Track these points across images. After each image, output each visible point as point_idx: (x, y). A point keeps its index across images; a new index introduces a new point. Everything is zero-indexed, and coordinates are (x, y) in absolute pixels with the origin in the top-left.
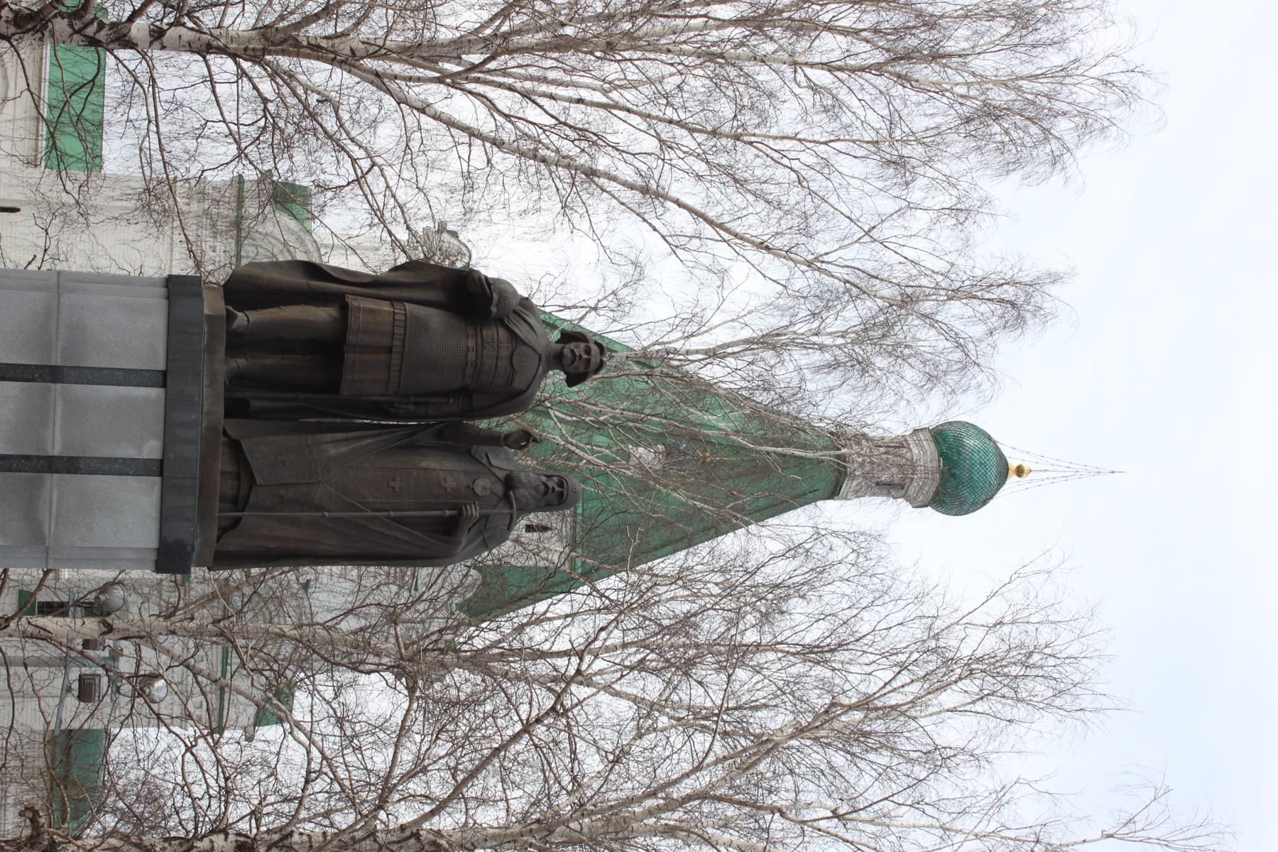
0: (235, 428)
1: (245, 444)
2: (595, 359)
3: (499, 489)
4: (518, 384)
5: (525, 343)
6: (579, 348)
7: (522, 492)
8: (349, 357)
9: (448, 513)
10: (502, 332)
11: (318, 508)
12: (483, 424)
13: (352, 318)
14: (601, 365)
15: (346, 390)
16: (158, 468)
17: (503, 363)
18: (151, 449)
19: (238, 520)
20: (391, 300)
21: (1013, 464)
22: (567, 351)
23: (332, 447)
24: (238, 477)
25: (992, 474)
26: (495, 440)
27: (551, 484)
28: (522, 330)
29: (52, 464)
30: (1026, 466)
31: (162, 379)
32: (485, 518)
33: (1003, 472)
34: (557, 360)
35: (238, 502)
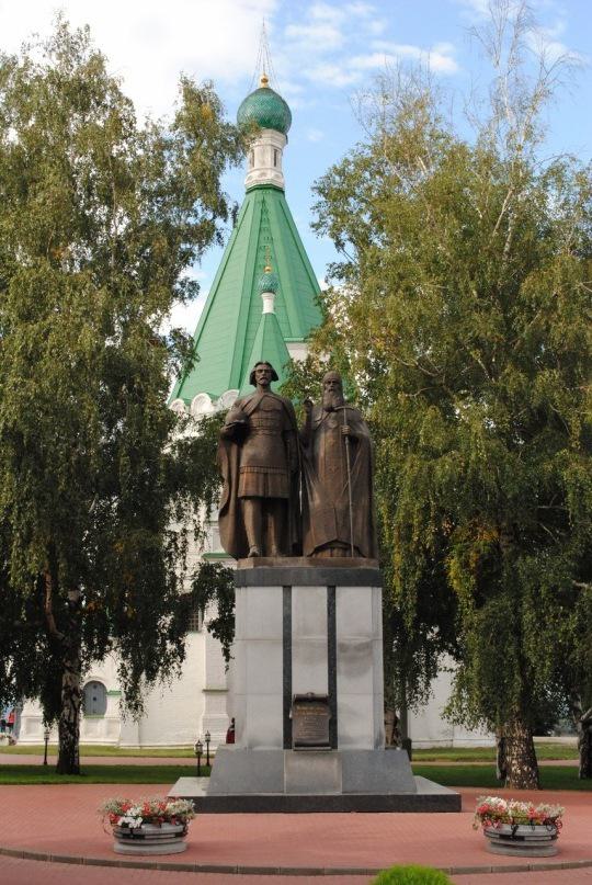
0: (308, 550)
3: (333, 414)
5: (259, 404)
6: (259, 376)
7: (334, 404)
9: (347, 441)
10: (252, 417)
11: (348, 509)
13: (250, 494)
14: (268, 364)
15: (287, 496)
17: (269, 414)
18: (323, 592)
19: (355, 547)
21: (262, 85)
22: (262, 382)
23: (316, 501)
24: (333, 548)
25: (266, 97)
26: (309, 419)
27: (329, 388)
28: (252, 407)
30: (262, 77)
31: (287, 588)
32: (349, 422)
33: (267, 90)
34: (266, 387)
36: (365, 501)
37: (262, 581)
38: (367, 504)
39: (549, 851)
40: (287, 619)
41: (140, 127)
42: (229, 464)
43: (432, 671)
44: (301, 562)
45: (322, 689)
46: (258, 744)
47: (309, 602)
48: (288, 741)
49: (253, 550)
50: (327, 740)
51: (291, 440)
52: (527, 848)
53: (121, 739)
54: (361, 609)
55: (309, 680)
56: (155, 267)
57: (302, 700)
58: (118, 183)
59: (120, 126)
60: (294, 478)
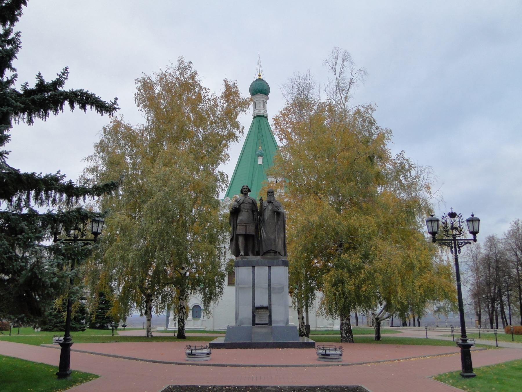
0: (261, 253)
1: (265, 251)
2: (246, 187)
3: (271, 204)
4: (251, 202)
8: (248, 233)
12: (258, 209)
15: (253, 234)
16: (269, 267)
20: (237, 226)
21: (258, 77)
29: (270, 285)
31: (253, 267)
34: (246, 194)
35: (275, 252)
36: (282, 235)
37: (245, 264)
38: (283, 236)
39: (339, 360)
40: (270, 279)
41: (28, 209)
42: (234, 223)
43: (313, 297)
44: (259, 258)
45: (266, 304)
46: (243, 324)
47: (262, 272)
48: (254, 323)
49: (242, 253)
50: (267, 322)
51: (255, 213)
52: (331, 358)
53: (206, 327)
54: (281, 274)
55: (262, 301)
56: (215, 149)
57: (258, 308)
58: (201, 120)
59: (200, 99)
60: (257, 228)
